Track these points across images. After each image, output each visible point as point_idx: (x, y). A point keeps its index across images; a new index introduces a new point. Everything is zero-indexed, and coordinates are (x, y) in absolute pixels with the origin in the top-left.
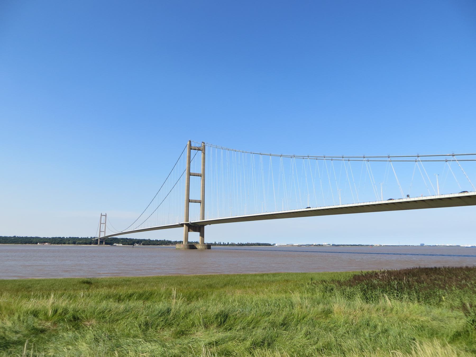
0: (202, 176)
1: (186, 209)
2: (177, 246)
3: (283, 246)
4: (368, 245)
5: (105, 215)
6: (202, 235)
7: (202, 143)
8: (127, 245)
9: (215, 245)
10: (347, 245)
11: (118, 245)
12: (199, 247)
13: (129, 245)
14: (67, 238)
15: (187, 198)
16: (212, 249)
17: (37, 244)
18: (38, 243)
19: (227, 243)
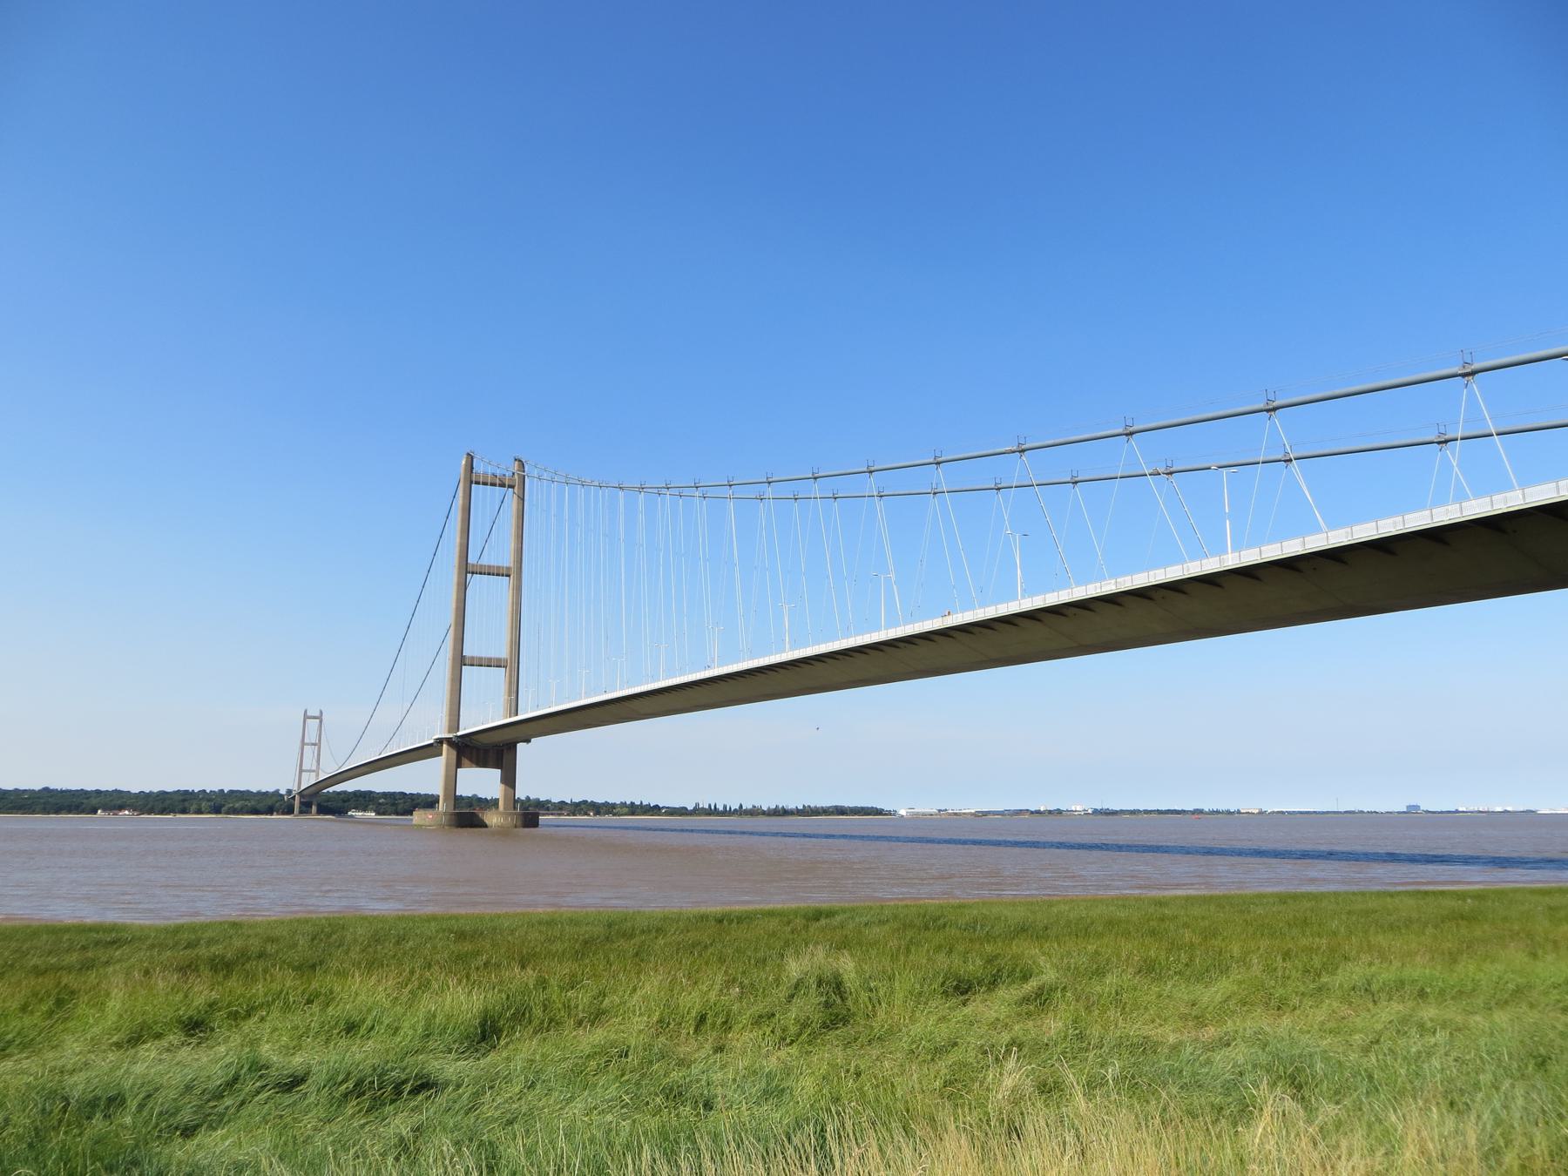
0: (513, 573)
1: (452, 690)
2: (419, 817)
3: (924, 814)
4: (1218, 812)
5: (317, 714)
6: (509, 780)
7: (516, 460)
8: (390, 814)
9: (709, 814)
10: (1146, 812)
11: (360, 814)
12: (495, 820)
13: (397, 814)
14: (528, 798)
15: (455, 649)
16: (543, 826)
17: (95, 812)
18: (99, 811)
19: (721, 808)
